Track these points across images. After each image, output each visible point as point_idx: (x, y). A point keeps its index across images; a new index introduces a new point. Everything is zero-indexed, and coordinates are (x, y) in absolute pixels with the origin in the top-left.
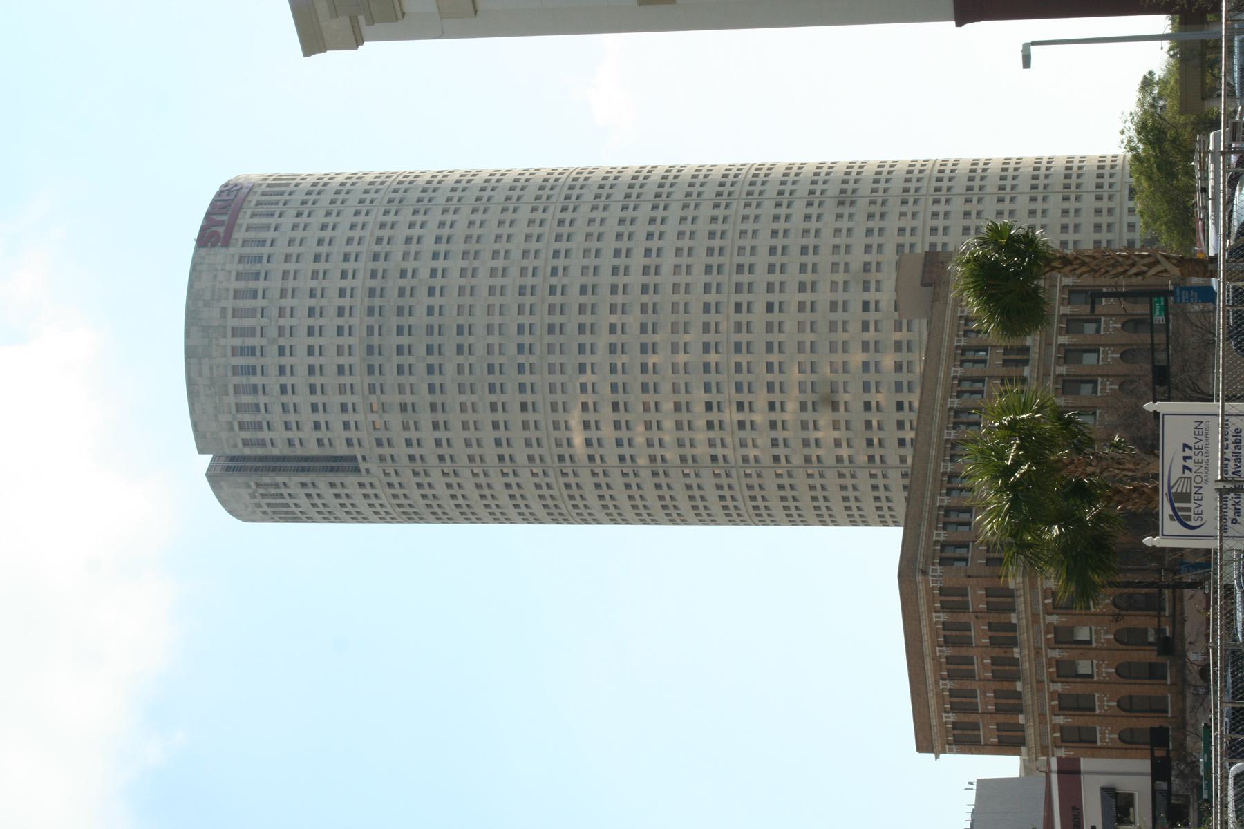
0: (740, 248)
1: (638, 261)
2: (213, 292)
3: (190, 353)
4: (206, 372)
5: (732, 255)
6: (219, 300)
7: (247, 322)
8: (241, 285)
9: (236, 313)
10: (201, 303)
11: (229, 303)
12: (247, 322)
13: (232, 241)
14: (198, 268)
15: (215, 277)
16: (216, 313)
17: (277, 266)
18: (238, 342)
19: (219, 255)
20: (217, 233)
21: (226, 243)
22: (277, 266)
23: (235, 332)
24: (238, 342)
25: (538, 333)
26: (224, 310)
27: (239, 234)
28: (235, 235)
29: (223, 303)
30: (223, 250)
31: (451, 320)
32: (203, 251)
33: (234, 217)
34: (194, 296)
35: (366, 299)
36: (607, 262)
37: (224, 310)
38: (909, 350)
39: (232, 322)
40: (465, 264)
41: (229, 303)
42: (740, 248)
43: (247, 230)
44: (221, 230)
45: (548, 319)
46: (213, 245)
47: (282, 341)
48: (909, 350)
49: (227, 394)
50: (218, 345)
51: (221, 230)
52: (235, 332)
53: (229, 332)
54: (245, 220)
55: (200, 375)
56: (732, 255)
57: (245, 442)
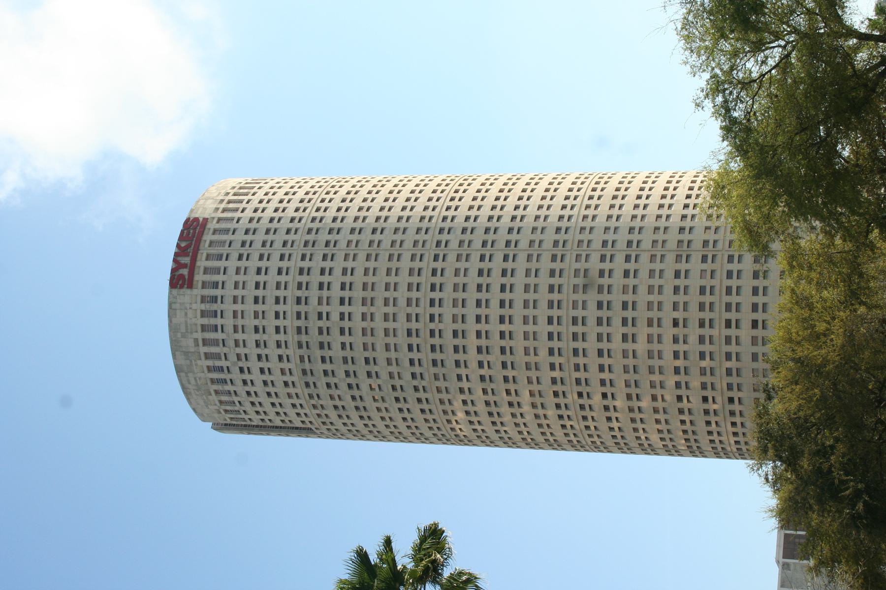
0: (579, 241)
1: (495, 311)
2: (187, 326)
3: (179, 370)
4: (193, 382)
5: (568, 309)
6: (191, 333)
7: (214, 350)
8: (205, 321)
9: (205, 342)
10: (179, 335)
11: (199, 335)
12: (214, 350)
13: (195, 283)
14: (174, 306)
15: (186, 314)
16: (191, 343)
17: (231, 278)
18: (210, 363)
19: (187, 296)
20: (182, 276)
21: (190, 286)
22: (229, 292)
23: (207, 356)
24: (210, 363)
25: (425, 366)
26: (196, 340)
27: (199, 277)
28: (198, 264)
29: (195, 335)
30: (188, 291)
31: (359, 354)
32: (175, 291)
33: (194, 260)
34: (173, 329)
35: (296, 336)
36: (471, 311)
37: (196, 340)
38: (711, 326)
39: (203, 350)
40: (364, 309)
41: (199, 335)
42: (579, 241)
43: (207, 259)
44: (185, 272)
45: (432, 356)
46: (182, 287)
47: (241, 364)
48: (711, 326)
49: (211, 395)
50: (196, 365)
51: (185, 272)
52: (207, 356)
53: (203, 357)
54: (208, 237)
55: (189, 383)
56: (568, 309)
57: (231, 419)
